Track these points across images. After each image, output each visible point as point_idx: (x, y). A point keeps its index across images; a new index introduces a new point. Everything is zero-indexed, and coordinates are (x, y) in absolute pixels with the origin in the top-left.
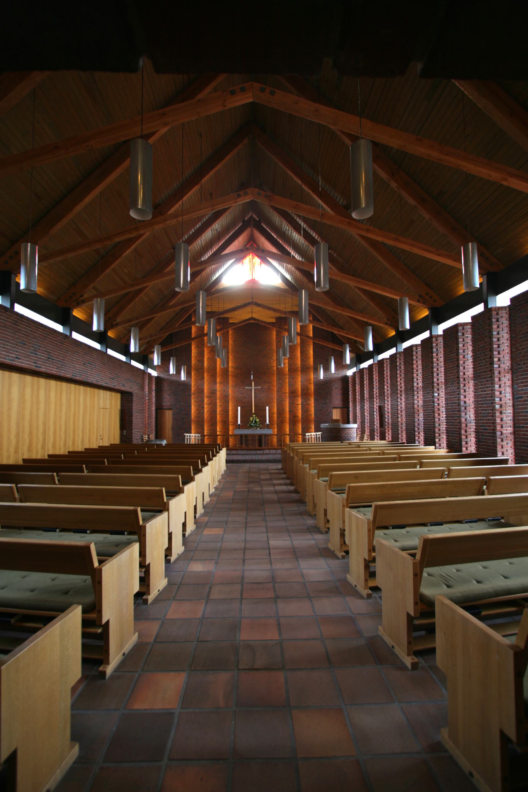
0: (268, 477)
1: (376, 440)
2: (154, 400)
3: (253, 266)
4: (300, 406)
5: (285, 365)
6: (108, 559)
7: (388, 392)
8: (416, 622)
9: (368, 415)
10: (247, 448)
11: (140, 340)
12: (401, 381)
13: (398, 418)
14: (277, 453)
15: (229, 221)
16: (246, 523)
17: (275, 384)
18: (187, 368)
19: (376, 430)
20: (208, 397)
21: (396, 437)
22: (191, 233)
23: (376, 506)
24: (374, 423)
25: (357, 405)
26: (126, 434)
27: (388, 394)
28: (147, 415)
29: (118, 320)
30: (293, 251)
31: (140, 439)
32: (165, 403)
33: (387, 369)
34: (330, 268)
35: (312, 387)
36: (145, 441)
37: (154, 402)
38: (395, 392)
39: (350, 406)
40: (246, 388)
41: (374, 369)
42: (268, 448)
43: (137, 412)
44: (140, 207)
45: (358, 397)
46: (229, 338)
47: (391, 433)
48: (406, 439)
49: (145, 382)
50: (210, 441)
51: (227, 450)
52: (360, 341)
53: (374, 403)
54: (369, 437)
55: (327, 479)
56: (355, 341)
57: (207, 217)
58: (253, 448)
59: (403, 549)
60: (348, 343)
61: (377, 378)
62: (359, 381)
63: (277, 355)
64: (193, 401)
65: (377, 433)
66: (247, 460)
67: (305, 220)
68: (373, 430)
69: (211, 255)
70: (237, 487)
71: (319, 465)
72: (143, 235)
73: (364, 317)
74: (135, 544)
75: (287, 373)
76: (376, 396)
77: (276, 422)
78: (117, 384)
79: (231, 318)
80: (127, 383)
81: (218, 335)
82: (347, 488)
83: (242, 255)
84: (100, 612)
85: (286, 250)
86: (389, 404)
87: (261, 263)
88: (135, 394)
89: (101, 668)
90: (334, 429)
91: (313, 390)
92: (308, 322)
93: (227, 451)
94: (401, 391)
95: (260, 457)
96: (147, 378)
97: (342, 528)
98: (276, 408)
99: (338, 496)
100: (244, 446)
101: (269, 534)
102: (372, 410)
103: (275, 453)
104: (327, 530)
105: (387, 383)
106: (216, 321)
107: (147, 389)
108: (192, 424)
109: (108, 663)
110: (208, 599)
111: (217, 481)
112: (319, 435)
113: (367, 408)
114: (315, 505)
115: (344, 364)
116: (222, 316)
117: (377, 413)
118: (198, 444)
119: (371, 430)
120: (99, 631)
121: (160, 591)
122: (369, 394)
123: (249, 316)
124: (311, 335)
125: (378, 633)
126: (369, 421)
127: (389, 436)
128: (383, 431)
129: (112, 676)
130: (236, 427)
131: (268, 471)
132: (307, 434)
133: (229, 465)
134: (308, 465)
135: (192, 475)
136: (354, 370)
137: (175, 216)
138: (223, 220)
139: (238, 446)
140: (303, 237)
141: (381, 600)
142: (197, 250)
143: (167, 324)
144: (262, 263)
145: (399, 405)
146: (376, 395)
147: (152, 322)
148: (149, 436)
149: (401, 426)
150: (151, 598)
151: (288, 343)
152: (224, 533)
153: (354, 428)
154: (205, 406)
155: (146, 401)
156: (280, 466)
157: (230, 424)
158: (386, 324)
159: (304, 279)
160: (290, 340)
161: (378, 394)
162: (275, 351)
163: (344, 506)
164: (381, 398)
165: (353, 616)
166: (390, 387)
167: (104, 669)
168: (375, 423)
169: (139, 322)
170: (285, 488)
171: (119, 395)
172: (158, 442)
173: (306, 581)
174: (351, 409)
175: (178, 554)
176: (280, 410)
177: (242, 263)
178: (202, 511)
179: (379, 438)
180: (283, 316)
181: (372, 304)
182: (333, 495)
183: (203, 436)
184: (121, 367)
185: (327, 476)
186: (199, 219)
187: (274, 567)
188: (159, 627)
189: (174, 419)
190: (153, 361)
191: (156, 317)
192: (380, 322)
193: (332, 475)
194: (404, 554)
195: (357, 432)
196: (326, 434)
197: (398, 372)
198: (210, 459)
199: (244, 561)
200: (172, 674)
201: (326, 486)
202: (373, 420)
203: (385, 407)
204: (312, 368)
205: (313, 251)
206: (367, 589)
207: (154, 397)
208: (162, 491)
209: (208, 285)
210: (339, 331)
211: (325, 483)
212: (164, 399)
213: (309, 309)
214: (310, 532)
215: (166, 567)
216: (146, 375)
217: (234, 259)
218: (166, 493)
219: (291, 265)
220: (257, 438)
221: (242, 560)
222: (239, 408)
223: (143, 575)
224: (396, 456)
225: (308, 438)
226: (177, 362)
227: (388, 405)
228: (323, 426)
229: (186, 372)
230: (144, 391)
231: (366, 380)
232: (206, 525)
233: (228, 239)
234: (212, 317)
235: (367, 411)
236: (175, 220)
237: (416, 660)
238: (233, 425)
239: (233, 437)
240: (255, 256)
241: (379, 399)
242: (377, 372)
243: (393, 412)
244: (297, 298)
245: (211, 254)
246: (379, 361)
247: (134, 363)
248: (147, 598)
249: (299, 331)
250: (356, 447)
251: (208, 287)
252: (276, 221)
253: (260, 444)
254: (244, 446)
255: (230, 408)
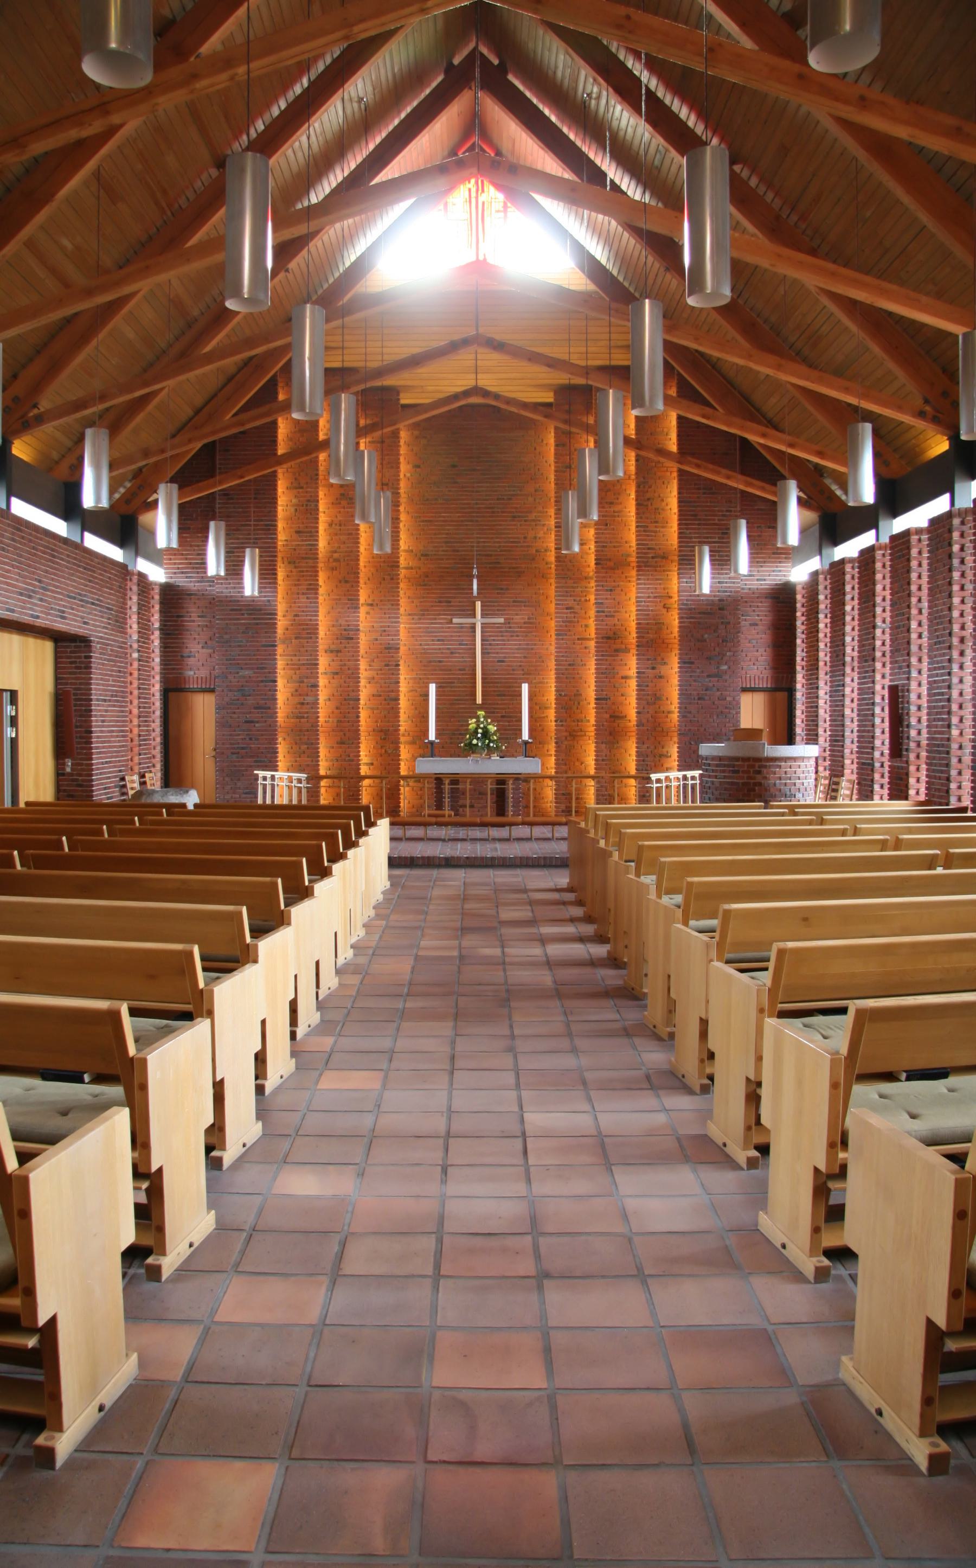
0: (523, 913)
1: (876, 797)
2: (157, 660)
3: (479, 215)
4: (633, 684)
5: (586, 547)
6: (45, 1150)
7: (919, 641)
8: (952, 1345)
9: (855, 715)
10: (458, 819)
11: (112, 466)
12: (963, 607)
13: (949, 726)
14: (557, 835)
15: (401, 69)
16: (453, 1058)
17: (552, 608)
18: (261, 556)
19: (877, 765)
20: (329, 651)
21: (939, 790)
22: (275, 112)
23: (860, 1013)
24: (873, 742)
25: (821, 684)
26: (72, 769)
27: (920, 648)
28: (135, 711)
29: (45, 404)
30: (614, 165)
31: (115, 787)
32: (191, 669)
33: (920, 565)
34: (736, 226)
35: (674, 621)
36: (131, 792)
37: (158, 669)
38: (944, 642)
39: (799, 686)
40: (455, 620)
41: (878, 565)
42: (527, 819)
43: (105, 701)
44: (113, 45)
45: (824, 656)
46: (399, 454)
47: (927, 776)
48: (972, 795)
49: (129, 603)
50: (338, 795)
51: (392, 824)
52: (834, 470)
53: (874, 677)
54: (856, 786)
55: (714, 923)
56: (819, 470)
57: (329, 60)
58: (478, 820)
59: (931, 1141)
60: (795, 477)
61: (887, 593)
62: (828, 601)
63: (558, 511)
64: (280, 664)
65: (882, 776)
66: (459, 858)
67: (653, 65)
68: (869, 764)
69: (342, 182)
70: (423, 943)
71: (690, 879)
72: (121, 126)
73: (847, 390)
74: (118, 1112)
75: (591, 574)
76: (884, 655)
77: (553, 735)
78: (41, 612)
79: (407, 388)
80: (73, 609)
81: (362, 447)
82: (773, 955)
83: (441, 182)
84: (30, 1292)
85: (591, 163)
86: (924, 682)
87: (505, 207)
88: (98, 643)
89: (41, 1440)
90: (745, 759)
91: (676, 630)
92: (660, 406)
93: (391, 829)
94: (962, 640)
95: (502, 850)
96: (135, 588)
97: (752, 1077)
98: (553, 689)
99: (744, 977)
100: (447, 811)
101: (524, 1094)
102: (870, 699)
103: (550, 835)
104: (707, 1081)
105: (920, 612)
106: (357, 400)
107: (135, 626)
108: (280, 740)
109: (59, 1428)
110: (336, 1276)
111: (359, 925)
112: (693, 778)
113: (853, 691)
114: (671, 1007)
115: (779, 545)
116: (378, 383)
117: (883, 710)
118: (299, 807)
119: (863, 764)
120: (32, 1342)
121: (196, 1245)
122: (859, 647)
123: (464, 383)
124: (674, 448)
125: (840, 1375)
126: (858, 737)
127: (918, 786)
128: (902, 768)
129: (70, 1463)
130: (421, 751)
131: (525, 896)
132: (654, 777)
133: (398, 872)
134: (654, 877)
135: (282, 907)
136: (814, 564)
137: (225, 61)
138: (381, 65)
139: (427, 812)
140: (646, 120)
141: (855, 1282)
142: (295, 168)
143: (198, 412)
144: (509, 205)
145: (953, 687)
146: (883, 648)
147: (151, 407)
148: (142, 776)
149: (959, 753)
150: (169, 1263)
151: (596, 472)
152: (384, 1086)
153: (809, 758)
154: (322, 681)
155: (131, 665)
156: (562, 879)
157: (402, 739)
158: (921, 415)
159: (650, 259)
160: (604, 467)
161: (887, 648)
162: (553, 500)
163: (761, 1011)
164: (896, 662)
165: (770, 1328)
166: (929, 626)
167: (49, 1444)
168: (877, 743)
169: (107, 409)
170: (578, 950)
171: (48, 647)
172: (173, 798)
173: (634, 1231)
174: (800, 695)
175: (244, 1145)
176: (565, 695)
177: (441, 207)
178: (316, 1018)
179: (886, 792)
180: (581, 381)
181: (876, 349)
182: (730, 975)
183: (315, 779)
184: (54, 556)
185: (713, 916)
186: (303, 67)
187: (539, 1188)
188: (195, 1342)
189: (222, 724)
190: (152, 533)
191: (162, 389)
192: (900, 408)
193: (727, 913)
194: (933, 1155)
195: (817, 772)
196: (716, 777)
197: (956, 575)
198: (337, 857)
199: (445, 1171)
200: (239, 1464)
201: (708, 946)
202: (868, 731)
203: (908, 691)
204: (676, 558)
205: (680, 166)
206: (818, 1256)
207: (157, 651)
208: (190, 954)
209: (331, 281)
210: (764, 435)
211: (704, 937)
212: (189, 657)
213: (665, 359)
214: (652, 1087)
215: (208, 1180)
216: (131, 580)
217: (414, 199)
218: (203, 959)
219: (605, 214)
220: (489, 786)
221: (440, 1168)
222: (432, 688)
223: (143, 1199)
224: (938, 852)
225: (657, 788)
226: (230, 534)
227: (920, 685)
228: (706, 749)
229: (260, 565)
230: (126, 633)
231: (853, 599)
232: (328, 1061)
233: (396, 128)
234: (344, 388)
235: (852, 701)
236: (224, 76)
237: (943, 1447)
238: (412, 743)
239: (411, 782)
240: (486, 183)
241: (891, 663)
242: (888, 575)
243: (935, 707)
244: (626, 323)
245: (340, 179)
246: (893, 538)
247: (93, 542)
248: (157, 1263)
249: (632, 432)
250: (810, 823)
251: (330, 286)
252: (556, 67)
253: (501, 809)
254: (447, 811)
255: (403, 688)
